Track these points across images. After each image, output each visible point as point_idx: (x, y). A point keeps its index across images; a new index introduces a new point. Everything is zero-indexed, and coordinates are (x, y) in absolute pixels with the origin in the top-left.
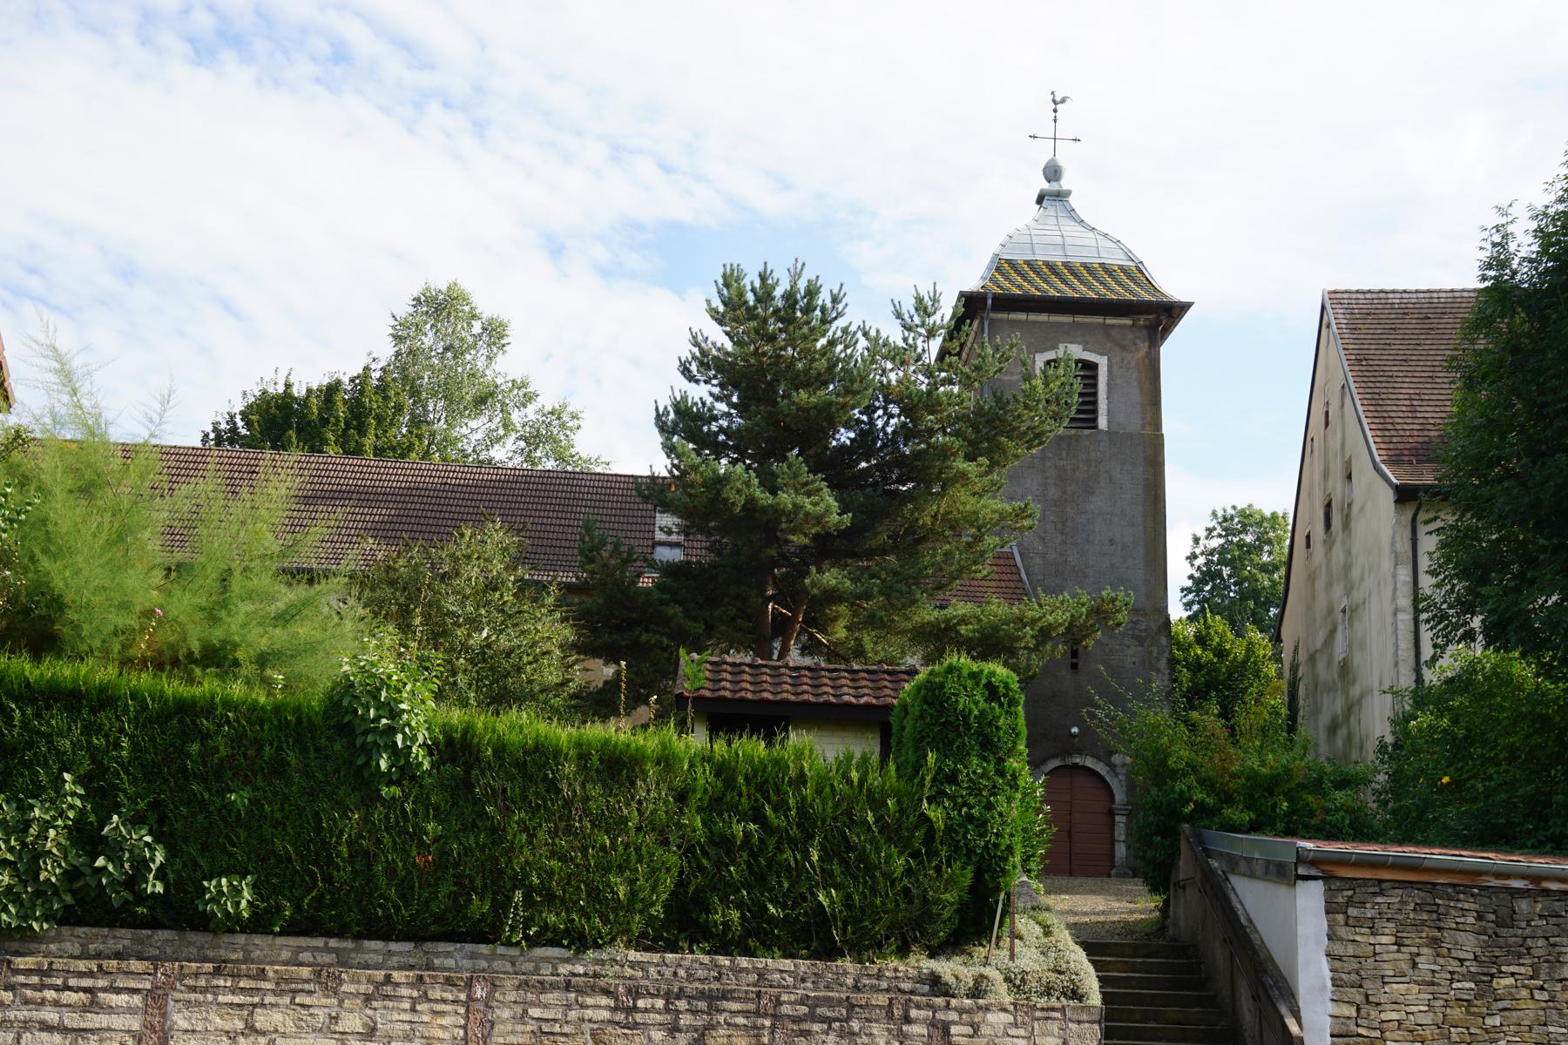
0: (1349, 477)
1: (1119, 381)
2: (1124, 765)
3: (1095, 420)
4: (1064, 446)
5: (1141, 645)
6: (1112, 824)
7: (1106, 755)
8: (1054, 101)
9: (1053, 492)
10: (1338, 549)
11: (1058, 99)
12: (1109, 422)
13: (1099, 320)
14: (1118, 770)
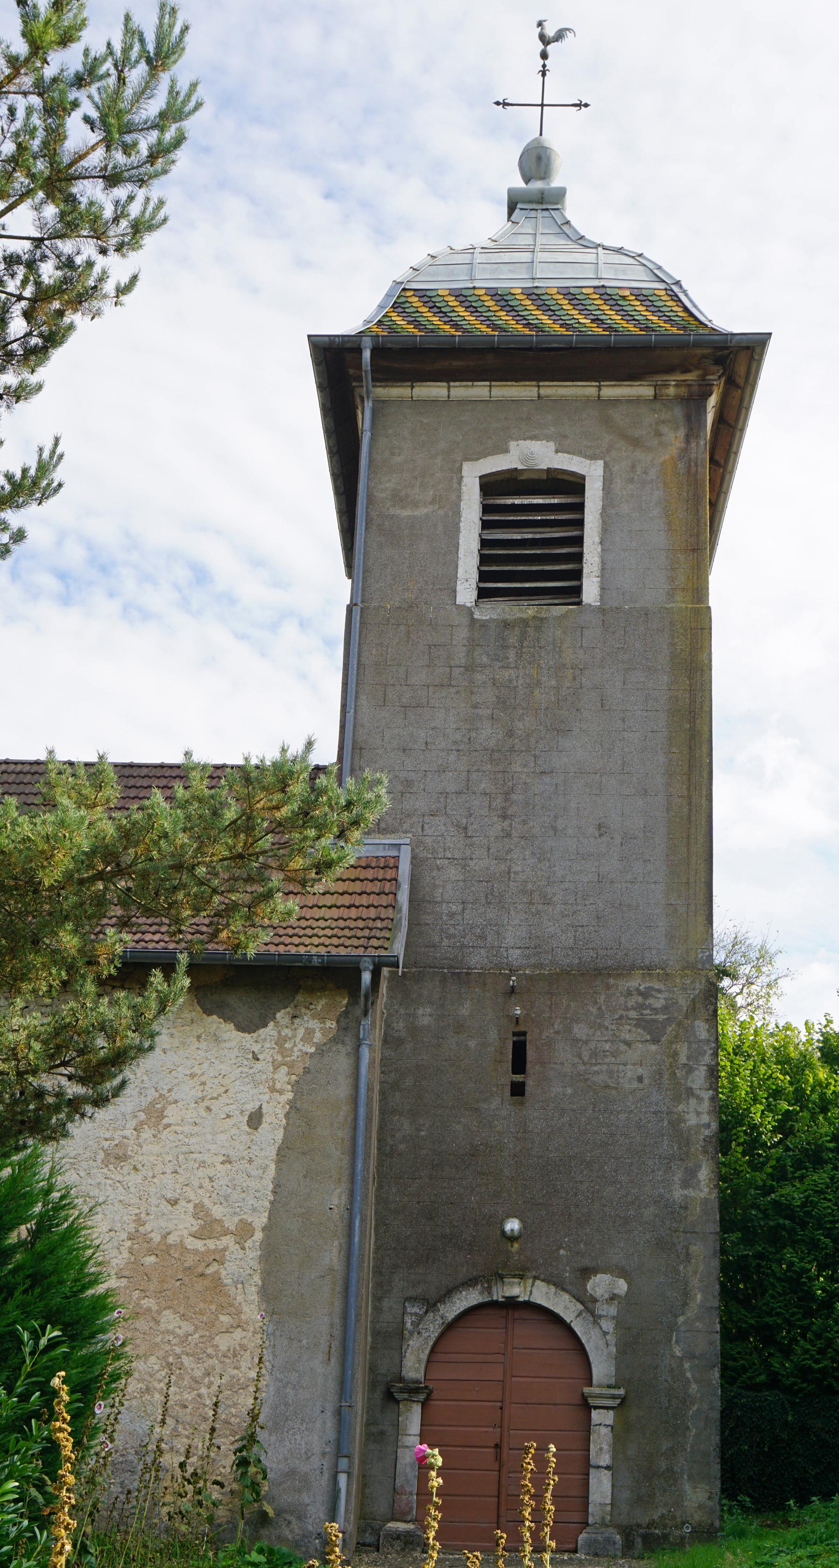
1: (625, 508)
2: (613, 1297)
3: (577, 591)
4: (513, 639)
5: (656, 1041)
6: (587, 1428)
8: (542, 38)
9: (488, 734)
11: (550, 32)
12: (603, 589)
14: (603, 1309)
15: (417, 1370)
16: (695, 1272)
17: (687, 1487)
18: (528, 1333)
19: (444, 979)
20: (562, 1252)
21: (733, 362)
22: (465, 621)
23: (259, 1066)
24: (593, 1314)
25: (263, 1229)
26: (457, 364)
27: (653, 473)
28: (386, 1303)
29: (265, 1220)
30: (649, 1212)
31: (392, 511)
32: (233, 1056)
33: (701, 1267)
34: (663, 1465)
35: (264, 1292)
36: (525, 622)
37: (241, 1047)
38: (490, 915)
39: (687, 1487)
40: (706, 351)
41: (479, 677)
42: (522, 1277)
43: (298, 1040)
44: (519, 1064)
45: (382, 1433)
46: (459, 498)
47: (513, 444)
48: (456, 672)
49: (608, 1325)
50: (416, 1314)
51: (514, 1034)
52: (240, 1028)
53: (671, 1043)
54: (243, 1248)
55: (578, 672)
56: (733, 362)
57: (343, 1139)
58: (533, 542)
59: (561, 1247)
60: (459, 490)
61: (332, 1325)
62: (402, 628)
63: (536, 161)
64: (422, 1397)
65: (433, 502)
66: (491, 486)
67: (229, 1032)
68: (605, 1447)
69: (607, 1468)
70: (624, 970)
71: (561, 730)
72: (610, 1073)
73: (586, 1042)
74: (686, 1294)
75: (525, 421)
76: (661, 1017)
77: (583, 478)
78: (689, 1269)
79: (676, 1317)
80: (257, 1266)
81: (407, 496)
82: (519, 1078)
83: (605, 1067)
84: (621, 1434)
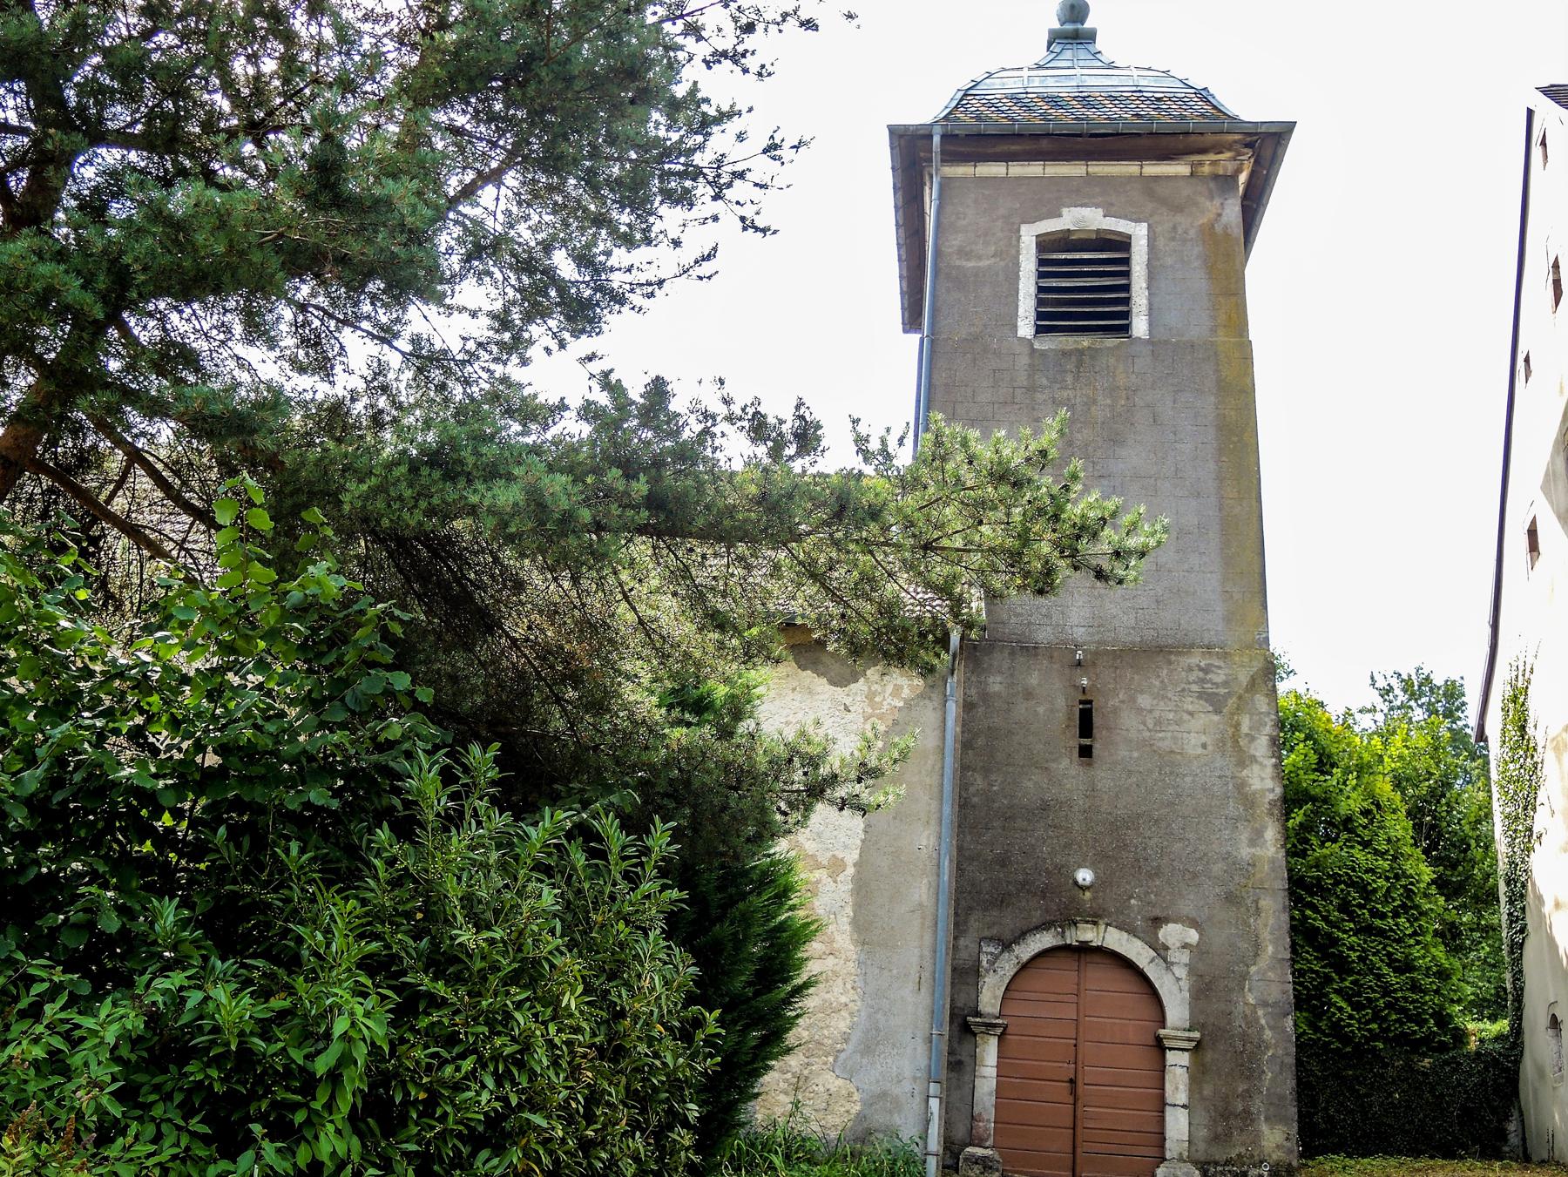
2: (1185, 946)
3: (1125, 329)
5: (1218, 711)
12: (1150, 324)
13: (1132, 168)
14: (1173, 956)
15: (993, 1006)
17: (1264, 1128)
18: (1099, 978)
19: (1012, 653)
21: (1267, 143)
22: (1026, 350)
23: (850, 716)
24: (1165, 960)
25: (855, 865)
27: (1192, 233)
28: (962, 942)
30: (1218, 868)
31: (958, 263)
33: (1271, 921)
35: (855, 922)
36: (1081, 352)
39: (1264, 1128)
40: (1237, 137)
41: (1040, 397)
42: (1095, 923)
45: (960, 1063)
46: (1018, 253)
47: (1065, 211)
48: (1018, 391)
49: (1181, 972)
52: (833, 683)
56: (1267, 143)
58: (1085, 290)
59: (1131, 897)
60: (1018, 246)
61: (921, 957)
64: (999, 1031)
66: (1046, 244)
67: (821, 684)
68: (1181, 1087)
69: (1184, 1106)
71: (1116, 440)
72: (1174, 738)
73: (1151, 711)
74: (1257, 947)
75: (1079, 193)
76: (1222, 691)
77: (1130, 237)
80: (849, 899)
82: (1086, 741)
84: (1197, 1075)
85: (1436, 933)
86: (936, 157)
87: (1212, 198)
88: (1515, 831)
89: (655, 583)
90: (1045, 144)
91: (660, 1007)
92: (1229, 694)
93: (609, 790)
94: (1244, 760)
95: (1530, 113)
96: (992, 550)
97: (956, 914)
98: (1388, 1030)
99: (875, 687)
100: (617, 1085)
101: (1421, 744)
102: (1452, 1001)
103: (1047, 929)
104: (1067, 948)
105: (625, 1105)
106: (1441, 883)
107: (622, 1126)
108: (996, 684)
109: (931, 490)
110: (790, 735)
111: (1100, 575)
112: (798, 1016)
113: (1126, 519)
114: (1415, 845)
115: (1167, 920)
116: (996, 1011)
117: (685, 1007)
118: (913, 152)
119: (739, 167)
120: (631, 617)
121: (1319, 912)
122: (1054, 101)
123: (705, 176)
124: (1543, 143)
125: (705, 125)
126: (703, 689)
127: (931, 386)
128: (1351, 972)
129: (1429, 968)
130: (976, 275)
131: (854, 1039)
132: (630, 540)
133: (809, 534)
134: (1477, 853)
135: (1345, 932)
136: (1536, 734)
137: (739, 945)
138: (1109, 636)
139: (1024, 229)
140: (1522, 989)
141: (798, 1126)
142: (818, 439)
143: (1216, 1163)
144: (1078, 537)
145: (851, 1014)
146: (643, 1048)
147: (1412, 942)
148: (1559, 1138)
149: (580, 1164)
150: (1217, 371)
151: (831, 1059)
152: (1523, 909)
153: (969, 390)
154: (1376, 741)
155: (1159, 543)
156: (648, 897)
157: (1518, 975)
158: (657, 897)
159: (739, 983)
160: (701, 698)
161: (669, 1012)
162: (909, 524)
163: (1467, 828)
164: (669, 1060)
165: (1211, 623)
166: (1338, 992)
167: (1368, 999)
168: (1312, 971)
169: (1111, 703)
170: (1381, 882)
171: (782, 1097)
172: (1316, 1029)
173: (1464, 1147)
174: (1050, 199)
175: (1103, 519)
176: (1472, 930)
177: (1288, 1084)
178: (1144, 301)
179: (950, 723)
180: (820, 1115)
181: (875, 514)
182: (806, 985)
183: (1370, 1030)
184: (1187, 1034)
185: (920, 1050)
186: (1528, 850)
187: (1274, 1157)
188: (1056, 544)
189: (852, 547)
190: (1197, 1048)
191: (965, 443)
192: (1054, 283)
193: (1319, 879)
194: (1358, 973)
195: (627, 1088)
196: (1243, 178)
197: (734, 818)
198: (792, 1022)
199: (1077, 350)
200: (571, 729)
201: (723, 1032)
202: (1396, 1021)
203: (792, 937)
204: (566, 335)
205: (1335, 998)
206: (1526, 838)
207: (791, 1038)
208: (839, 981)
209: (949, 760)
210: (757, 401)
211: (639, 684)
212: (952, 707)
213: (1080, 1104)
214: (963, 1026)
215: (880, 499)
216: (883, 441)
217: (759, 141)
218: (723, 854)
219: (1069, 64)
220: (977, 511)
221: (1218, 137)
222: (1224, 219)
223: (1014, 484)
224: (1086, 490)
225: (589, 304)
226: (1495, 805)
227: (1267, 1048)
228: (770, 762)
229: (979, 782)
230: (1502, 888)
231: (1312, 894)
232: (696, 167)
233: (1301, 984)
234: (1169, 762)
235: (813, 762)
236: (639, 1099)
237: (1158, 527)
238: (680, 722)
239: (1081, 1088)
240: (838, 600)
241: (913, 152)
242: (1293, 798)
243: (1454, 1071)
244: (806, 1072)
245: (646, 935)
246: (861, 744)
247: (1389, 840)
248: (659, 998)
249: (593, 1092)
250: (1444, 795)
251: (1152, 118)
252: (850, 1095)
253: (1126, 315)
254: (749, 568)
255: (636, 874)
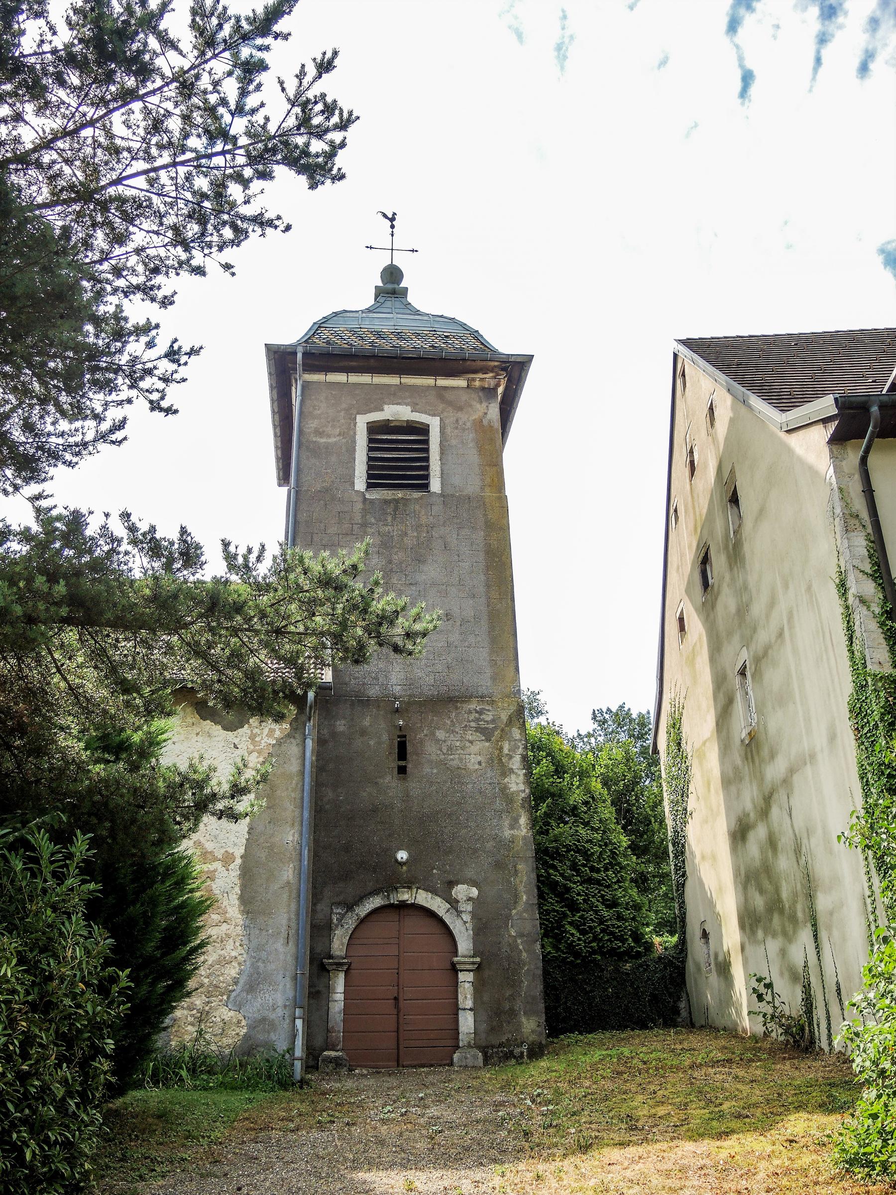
0: (734, 500)
2: (470, 899)
3: (426, 487)
6: (456, 984)
7: (445, 891)
10: (727, 601)
13: (429, 381)
14: (463, 907)
15: (341, 950)
16: (521, 882)
17: (524, 1020)
18: (413, 923)
19: (352, 704)
20: (435, 871)
21: (515, 369)
22: (360, 499)
25: (241, 857)
26: (354, 364)
27: (469, 425)
28: (319, 907)
29: (243, 851)
30: (490, 845)
31: (314, 439)
32: (220, 746)
33: (525, 879)
34: (507, 1006)
35: (243, 899)
36: (397, 501)
37: (226, 740)
38: (381, 666)
39: (524, 1020)
40: (496, 364)
42: (410, 888)
43: (264, 736)
44: (402, 754)
45: (318, 992)
47: (386, 407)
48: (355, 527)
49: (466, 917)
50: (339, 914)
51: (399, 737)
52: (225, 728)
53: (498, 741)
54: (228, 870)
55: (429, 529)
56: (515, 369)
57: (295, 798)
58: (399, 459)
59: (432, 869)
61: (289, 920)
62: (322, 502)
63: (392, 274)
64: (345, 968)
65: (339, 435)
66: (374, 429)
67: (217, 730)
68: (469, 996)
69: (471, 1009)
70: (466, 698)
71: (420, 560)
72: (461, 760)
73: (445, 741)
74: (516, 897)
76: (491, 726)
78: (517, 880)
79: (511, 910)
80: (237, 881)
81: (324, 432)
82: (402, 763)
83: (457, 756)
84: (479, 988)
85: (632, 880)
86: (299, 368)
87: (481, 402)
88: (677, 811)
89: (80, 660)
90: (372, 362)
91: (81, 970)
92: (495, 728)
93: (42, 812)
94: (506, 772)
95: (675, 356)
96: (322, 634)
97: (314, 887)
98: (603, 947)
99: (256, 731)
100: (48, 1030)
101: (619, 757)
102: (643, 924)
103: (377, 894)
104: (391, 906)
105: (56, 1045)
106: (633, 847)
107: (53, 1060)
108: (341, 726)
109: (280, 592)
110: (183, 767)
111: (397, 649)
112: (195, 969)
113: (414, 611)
114: (618, 823)
115: (457, 883)
116: (343, 953)
117: (103, 969)
118: (282, 363)
119: (149, 365)
120: (63, 684)
121: (558, 871)
122: (379, 335)
123: (123, 371)
124: (683, 375)
125: (120, 335)
126: (124, 735)
127: (296, 523)
128: (578, 910)
129: (628, 903)
130: (327, 448)
131: (242, 982)
132: (60, 629)
133: (192, 623)
134: (656, 826)
135: (575, 883)
136: (687, 748)
137: (148, 920)
138: (417, 692)
139: (359, 417)
140: (685, 913)
141: (201, 1047)
142: (198, 557)
143: (493, 1047)
144: (380, 624)
145: (239, 964)
146: (68, 1002)
147: (616, 887)
148: (711, 1010)
149: (18, 1091)
150: (485, 515)
151: (225, 997)
152: (683, 861)
153: (322, 525)
154: (590, 755)
155: (435, 627)
156: (72, 890)
157: (682, 905)
158: (79, 889)
159: (150, 947)
160: (122, 743)
161: (90, 973)
162: (263, 615)
163: (648, 810)
164: (89, 1008)
165: (484, 683)
166: (571, 923)
167: (590, 927)
168: (554, 910)
169: (418, 736)
170: (596, 848)
171: (190, 1028)
172: (557, 949)
173: (653, 1020)
174: (375, 398)
175: (396, 611)
176: (654, 876)
177: (538, 989)
178: (438, 468)
179: (308, 754)
180: (217, 1039)
181: (238, 608)
182: (202, 945)
183: (591, 947)
184: (471, 960)
185: (288, 986)
186: (685, 823)
187: (531, 1039)
188: (366, 629)
189: (223, 632)
190: (478, 969)
191: (301, 560)
192: (379, 455)
193: (557, 848)
194: (584, 911)
195: (56, 1032)
196: (500, 390)
197: (140, 828)
198: (189, 975)
199: (394, 499)
200: (18, 768)
201: (133, 985)
202: (607, 940)
203: (189, 911)
204: (19, 481)
205: (568, 927)
206: (683, 815)
207: (191, 984)
208: (231, 941)
209: (307, 779)
210: (153, 529)
211: (70, 734)
212: (309, 743)
213: (401, 1014)
214: (318, 967)
215: (242, 598)
216: (246, 558)
217: (162, 346)
218: (134, 855)
219: (389, 310)
220: (311, 607)
221: (484, 363)
222: (489, 417)
223: (336, 588)
224: (386, 592)
225: (33, 459)
226: (665, 794)
227: (524, 965)
228: (168, 787)
229: (330, 794)
230: (671, 848)
231: (553, 859)
232: (119, 365)
233: (547, 920)
234: (457, 775)
235: (200, 785)
236: (67, 1040)
237: (435, 616)
238: (97, 761)
239: (402, 1003)
240: (215, 667)
241: (282, 363)
242: (539, 794)
243: (645, 970)
244: (207, 1008)
245: (69, 918)
246: (234, 770)
247: (601, 821)
248: (80, 963)
249: (27, 1037)
250: (633, 790)
251: (442, 349)
252: (239, 1022)
253: (427, 477)
254: (150, 648)
255: (63, 873)
